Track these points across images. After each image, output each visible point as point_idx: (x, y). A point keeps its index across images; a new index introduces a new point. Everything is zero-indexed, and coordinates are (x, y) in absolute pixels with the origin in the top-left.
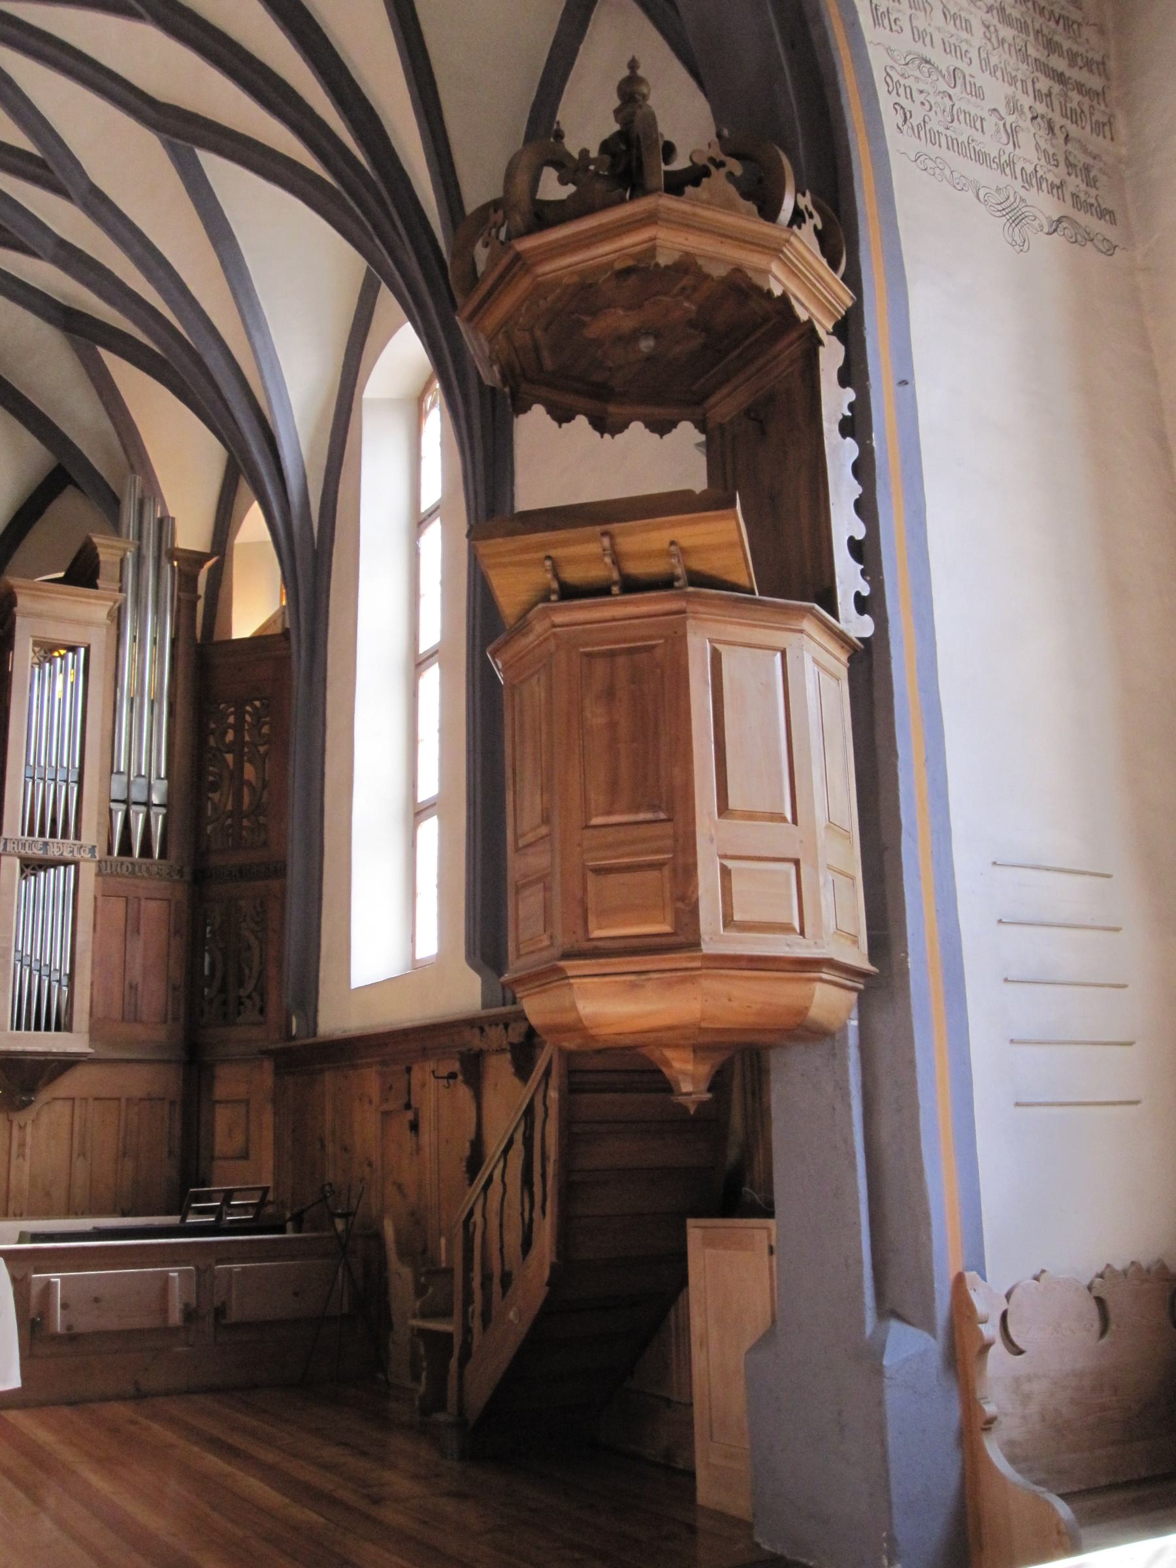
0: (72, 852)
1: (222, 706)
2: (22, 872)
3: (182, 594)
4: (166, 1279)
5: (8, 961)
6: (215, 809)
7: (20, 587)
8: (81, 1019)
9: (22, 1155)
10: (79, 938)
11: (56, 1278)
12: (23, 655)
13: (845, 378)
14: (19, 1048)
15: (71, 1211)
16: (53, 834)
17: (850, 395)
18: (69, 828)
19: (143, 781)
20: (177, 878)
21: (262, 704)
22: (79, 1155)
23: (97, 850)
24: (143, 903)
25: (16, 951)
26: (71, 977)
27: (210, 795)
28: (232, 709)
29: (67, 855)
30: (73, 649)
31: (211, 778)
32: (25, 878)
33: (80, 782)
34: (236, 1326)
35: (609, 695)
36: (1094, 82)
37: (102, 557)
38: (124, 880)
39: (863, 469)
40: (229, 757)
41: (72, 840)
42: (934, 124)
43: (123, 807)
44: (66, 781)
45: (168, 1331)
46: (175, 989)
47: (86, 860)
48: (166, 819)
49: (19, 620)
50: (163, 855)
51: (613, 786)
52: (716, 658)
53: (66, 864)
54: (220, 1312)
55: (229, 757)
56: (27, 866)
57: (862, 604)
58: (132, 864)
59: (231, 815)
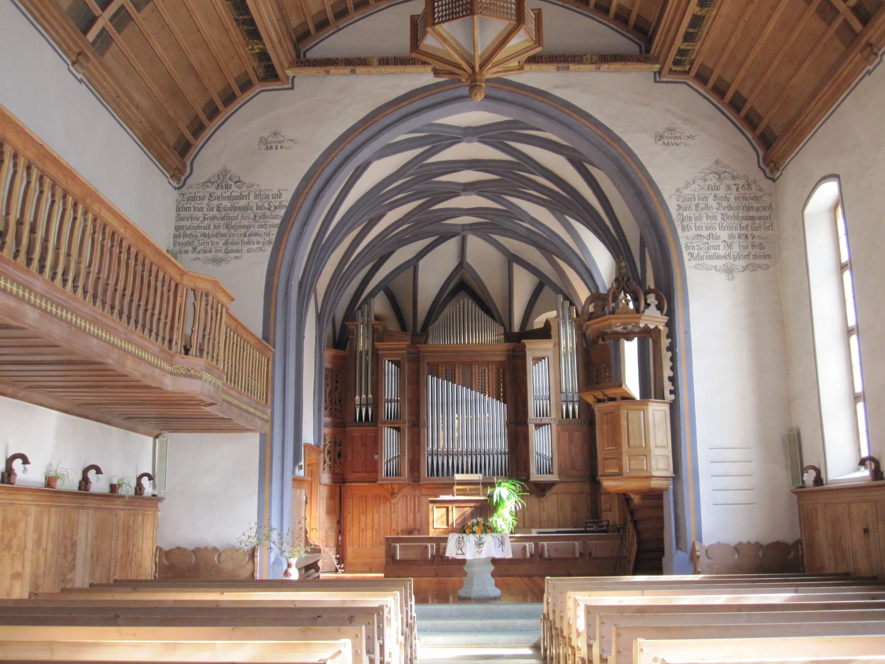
4: (574, 545)
11: (545, 543)
13: (668, 336)
15: (559, 527)
17: (669, 340)
33: (549, 399)
34: (596, 558)
35: (607, 422)
36: (766, 213)
39: (673, 359)
42: (702, 253)
45: (577, 559)
49: (527, 352)
51: (608, 443)
54: (590, 554)
57: (671, 392)
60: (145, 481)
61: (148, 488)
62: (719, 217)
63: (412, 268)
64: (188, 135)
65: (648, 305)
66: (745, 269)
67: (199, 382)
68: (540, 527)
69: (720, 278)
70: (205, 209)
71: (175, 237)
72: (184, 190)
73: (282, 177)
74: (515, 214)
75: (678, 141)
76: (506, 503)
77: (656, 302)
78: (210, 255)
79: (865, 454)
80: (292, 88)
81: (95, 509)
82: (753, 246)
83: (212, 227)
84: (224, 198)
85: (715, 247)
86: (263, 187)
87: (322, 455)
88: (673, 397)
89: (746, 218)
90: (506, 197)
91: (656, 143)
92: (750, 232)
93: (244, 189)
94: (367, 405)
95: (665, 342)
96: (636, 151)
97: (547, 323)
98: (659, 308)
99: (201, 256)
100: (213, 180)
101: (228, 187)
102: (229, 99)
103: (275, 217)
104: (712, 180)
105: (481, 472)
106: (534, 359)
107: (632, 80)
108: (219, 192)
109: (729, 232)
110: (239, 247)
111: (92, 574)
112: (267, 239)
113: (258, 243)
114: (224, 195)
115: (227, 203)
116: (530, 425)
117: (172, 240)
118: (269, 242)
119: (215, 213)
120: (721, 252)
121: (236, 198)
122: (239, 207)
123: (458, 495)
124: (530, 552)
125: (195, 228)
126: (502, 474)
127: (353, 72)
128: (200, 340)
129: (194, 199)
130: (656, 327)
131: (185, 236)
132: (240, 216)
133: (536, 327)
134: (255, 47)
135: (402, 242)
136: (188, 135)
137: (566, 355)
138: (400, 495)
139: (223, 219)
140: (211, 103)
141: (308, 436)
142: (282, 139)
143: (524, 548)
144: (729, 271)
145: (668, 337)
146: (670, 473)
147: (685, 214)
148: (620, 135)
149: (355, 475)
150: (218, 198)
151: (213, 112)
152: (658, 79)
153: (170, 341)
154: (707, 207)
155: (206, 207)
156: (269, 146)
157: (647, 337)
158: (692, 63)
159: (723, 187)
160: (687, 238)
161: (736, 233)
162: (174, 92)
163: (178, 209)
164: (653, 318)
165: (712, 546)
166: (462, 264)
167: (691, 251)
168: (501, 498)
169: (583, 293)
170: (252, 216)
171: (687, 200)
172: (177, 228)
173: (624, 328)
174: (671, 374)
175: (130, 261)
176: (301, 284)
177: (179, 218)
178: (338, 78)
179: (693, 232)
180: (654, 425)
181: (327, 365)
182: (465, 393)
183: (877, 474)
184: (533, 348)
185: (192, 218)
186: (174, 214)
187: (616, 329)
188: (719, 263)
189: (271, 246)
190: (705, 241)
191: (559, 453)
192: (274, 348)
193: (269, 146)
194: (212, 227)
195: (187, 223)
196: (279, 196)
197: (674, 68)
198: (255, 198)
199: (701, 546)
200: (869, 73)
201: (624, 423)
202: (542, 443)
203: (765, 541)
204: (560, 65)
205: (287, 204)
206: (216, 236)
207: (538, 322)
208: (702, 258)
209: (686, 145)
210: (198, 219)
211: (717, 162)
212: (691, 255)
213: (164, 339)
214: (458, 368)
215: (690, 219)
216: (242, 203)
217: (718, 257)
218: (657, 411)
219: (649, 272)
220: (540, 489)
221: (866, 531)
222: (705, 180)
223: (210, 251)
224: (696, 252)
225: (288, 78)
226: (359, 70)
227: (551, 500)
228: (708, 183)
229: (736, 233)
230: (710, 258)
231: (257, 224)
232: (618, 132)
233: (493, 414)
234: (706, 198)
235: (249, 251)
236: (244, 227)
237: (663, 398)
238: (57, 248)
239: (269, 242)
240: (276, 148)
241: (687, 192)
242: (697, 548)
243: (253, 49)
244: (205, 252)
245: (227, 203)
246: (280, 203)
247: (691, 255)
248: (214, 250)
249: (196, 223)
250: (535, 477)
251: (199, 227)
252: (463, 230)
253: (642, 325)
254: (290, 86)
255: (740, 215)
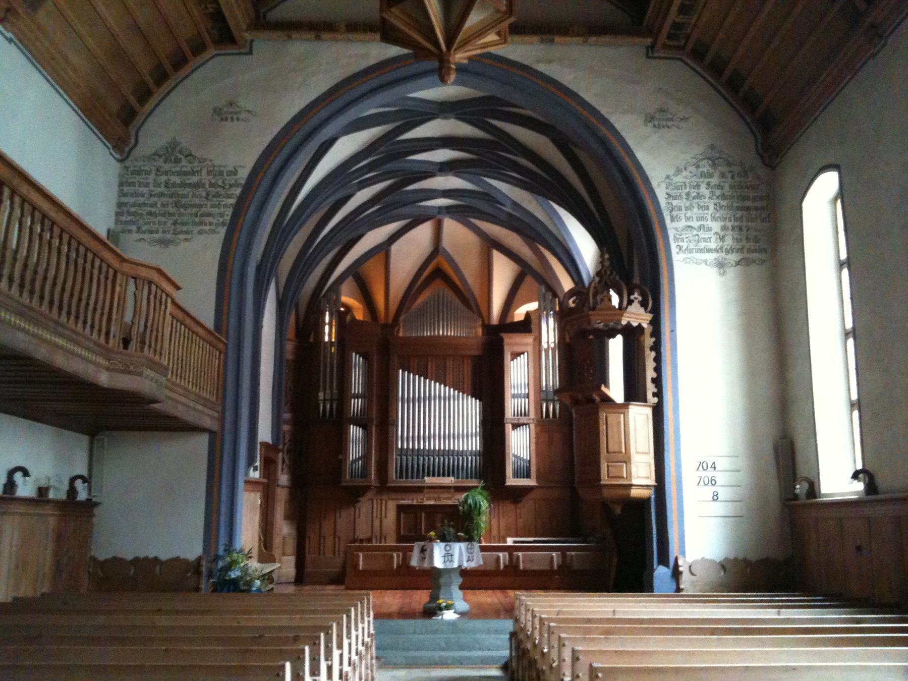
4: (552, 557)
11: (520, 554)
12: (507, 356)
17: (653, 339)
29: (525, 422)
33: (528, 397)
42: (692, 246)
52: (606, 417)
60: (79, 484)
61: (82, 495)
62: (712, 207)
64: (133, 100)
65: (630, 302)
66: (738, 263)
67: (139, 378)
68: (517, 536)
69: (712, 273)
70: (151, 185)
71: (118, 214)
72: (128, 163)
73: (240, 153)
74: (489, 197)
75: (670, 124)
77: (640, 298)
78: (156, 236)
79: (859, 466)
80: (250, 53)
81: (21, 514)
82: (748, 239)
83: (159, 205)
84: (173, 173)
85: (706, 240)
86: (217, 163)
87: (281, 454)
88: (656, 400)
89: (738, 208)
90: (486, 179)
91: (646, 125)
92: (745, 224)
93: (196, 164)
94: (331, 400)
95: (649, 341)
96: (623, 134)
97: (528, 315)
98: (644, 304)
99: (146, 236)
100: (161, 153)
101: (178, 161)
102: (180, 62)
103: (229, 197)
104: (706, 167)
105: (453, 475)
106: (512, 354)
107: (621, 54)
108: (167, 167)
109: (722, 223)
110: (190, 228)
111: (17, 587)
112: (221, 220)
113: (211, 224)
114: (174, 170)
115: (177, 179)
117: (113, 218)
118: (223, 224)
119: (162, 189)
120: (713, 245)
121: (186, 174)
122: (190, 184)
124: (504, 563)
125: (140, 205)
127: (318, 38)
128: (142, 329)
129: (138, 172)
130: (640, 325)
131: (129, 213)
132: (191, 194)
133: (516, 319)
134: (209, 6)
135: (374, 223)
136: (133, 100)
137: (547, 351)
139: (171, 196)
140: (160, 66)
141: (265, 433)
142: (238, 110)
143: (498, 558)
144: (721, 265)
145: (652, 336)
146: (652, 482)
147: (675, 203)
148: (606, 116)
150: (166, 173)
151: (161, 77)
152: (650, 54)
153: (108, 334)
154: (699, 196)
155: (151, 181)
156: (224, 117)
157: (632, 335)
158: (688, 37)
159: (717, 174)
160: (676, 229)
161: (729, 224)
162: (118, 54)
163: (121, 184)
164: (636, 315)
165: (696, 561)
166: (437, 249)
167: (681, 244)
169: (567, 284)
170: (204, 194)
171: (677, 188)
172: (120, 205)
173: (605, 325)
174: (655, 375)
175: (53, 241)
176: (259, 268)
177: (122, 194)
178: (300, 46)
179: (682, 223)
180: (635, 430)
181: (289, 356)
182: (438, 389)
183: (871, 488)
184: (512, 342)
185: (136, 194)
186: (116, 188)
187: (596, 326)
188: (711, 257)
189: (225, 228)
190: (695, 232)
191: (537, 456)
192: (227, 338)
193: (224, 117)
194: (159, 205)
195: (132, 200)
196: (235, 173)
197: (669, 43)
198: (208, 174)
199: (685, 561)
200: (873, 56)
201: (603, 427)
202: (520, 444)
203: (753, 557)
204: (544, 37)
205: (243, 182)
206: (163, 215)
207: (520, 313)
208: (691, 251)
209: (678, 128)
210: (143, 195)
211: (712, 147)
212: (680, 248)
213: (100, 331)
214: (431, 360)
215: (680, 209)
216: (194, 179)
217: (709, 251)
218: (639, 417)
219: (636, 261)
221: (859, 548)
222: (698, 167)
223: (157, 232)
224: (685, 245)
225: (246, 41)
226: (325, 36)
228: (701, 169)
229: (729, 224)
230: (701, 251)
231: (209, 204)
232: (604, 111)
233: (467, 412)
234: (698, 186)
235: (200, 233)
236: (195, 206)
237: (645, 401)
239: (223, 224)
240: (232, 119)
241: (679, 179)
242: (680, 562)
243: (206, 8)
244: (151, 232)
245: (177, 179)
246: (236, 181)
247: (680, 248)
248: (161, 230)
249: (141, 200)
251: (144, 204)
252: (439, 213)
253: (624, 322)
254: (248, 50)
255: (735, 205)
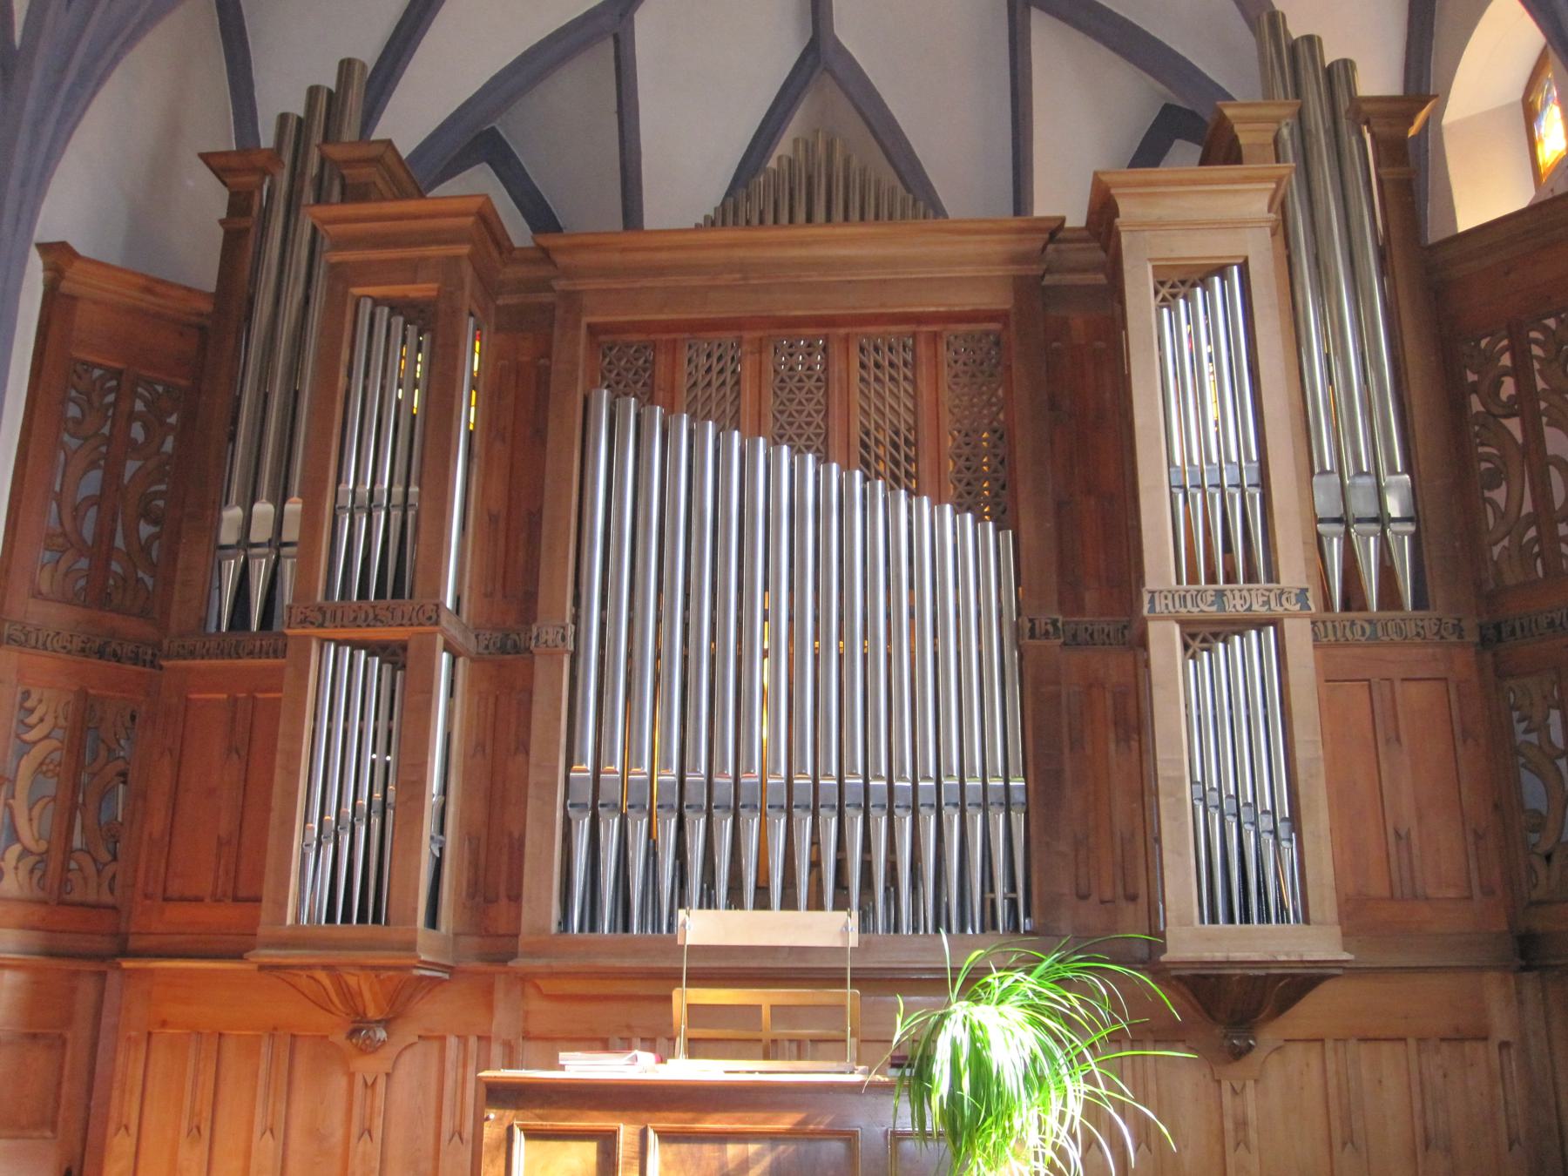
0: (1267, 602)
1: (1483, 343)
2: (1186, 647)
3: (1383, 171)
5: (1182, 801)
6: (1501, 516)
7: (1127, 185)
8: (1324, 902)
9: (1242, 1142)
10: (1301, 753)
14: (1219, 956)
16: (1230, 577)
18: (1258, 565)
19: (1368, 481)
20: (1453, 639)
21: (1561, 322)
22: (1344, 1144)
23: (1309, 594)
24: (1397, 684)
25: (1192, 782)
26: (1295, 820)
27: (1487, 494)
28: (1505, 342)
29: (1259, 608)
30: (1222, 271)
31: (1484, 465)
32: (1193, 657)
37: (1242, 141)
38: (1358, 651)
40: (1514, 425)
41: (1263, 584)
43: (1340, 528)
44: (1240, 486)
46: (1478, 836)
47: (1294, 616)
48: (1416, 539)
50: (1420, 602)
53: (1260, 625)
55: (1514, 425)
56: (1193, 636)
58: (1370, 622)
59: (1533, 519)
63: (608, 47)
76: (1024, 1116)
105: (841, 904)
116: (1154, 629)
123: (696, 1048)
126: (989, 923)
138: (408, 1032)
149: (177, 914)
168: (982, 1075)
202: (1229, 728)
220: (1231, 1009)
227: (1285, 1079)
238: (815, 865)
250: (1193, 938)
